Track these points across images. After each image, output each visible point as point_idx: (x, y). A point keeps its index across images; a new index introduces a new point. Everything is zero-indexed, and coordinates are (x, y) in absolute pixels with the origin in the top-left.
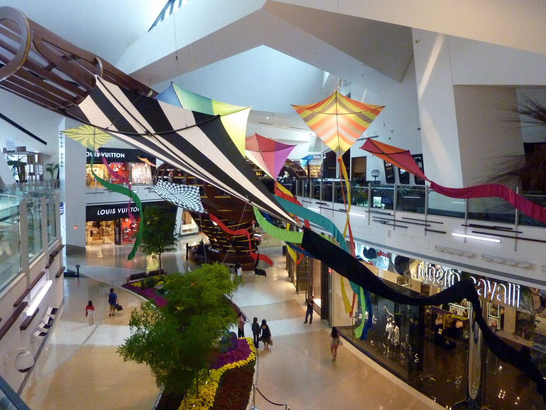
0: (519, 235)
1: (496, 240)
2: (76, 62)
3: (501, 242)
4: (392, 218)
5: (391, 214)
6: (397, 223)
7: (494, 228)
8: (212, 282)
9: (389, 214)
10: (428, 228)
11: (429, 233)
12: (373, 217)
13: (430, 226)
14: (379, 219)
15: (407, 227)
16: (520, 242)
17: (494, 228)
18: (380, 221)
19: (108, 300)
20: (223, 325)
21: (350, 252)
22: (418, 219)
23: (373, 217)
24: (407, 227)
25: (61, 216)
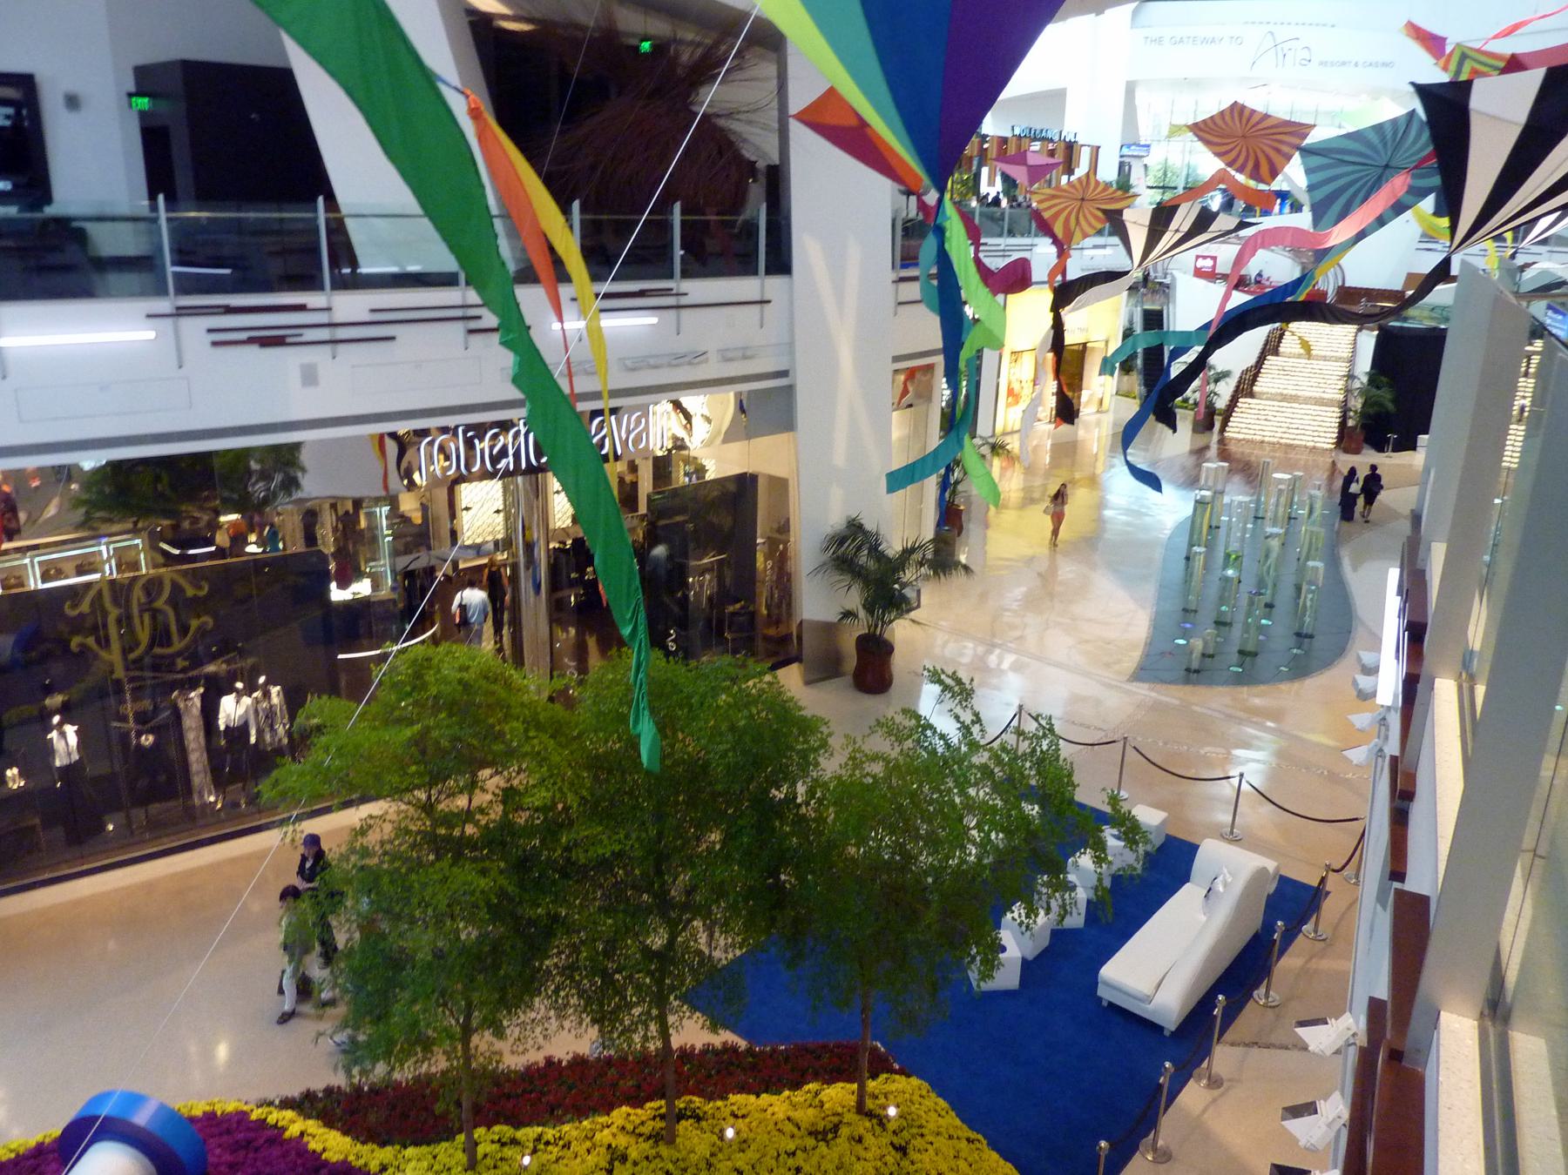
0: (684, 301)
1: (650, 319)
2: (1426, 505)
3: (15, 186)
4: (322, 318)
5: (309, 306)
6: (342, 333)
7: (642, 294)
8: (494, 687)
9: (301, 308)
10: (473, 325)
11: (477, 340)
12: (210, 331)
13: (479, 317)
14: (243, 336)
15: (393, 338)
16: (685, 313)
17: (642, 294)
18: (251, 341)
19: (1256, 101)
20: (277, 1102)
21: (1422, 279)
22: (434, 305)
23: (210, 331)
24: (393, 338)
25: (1228, 272)
